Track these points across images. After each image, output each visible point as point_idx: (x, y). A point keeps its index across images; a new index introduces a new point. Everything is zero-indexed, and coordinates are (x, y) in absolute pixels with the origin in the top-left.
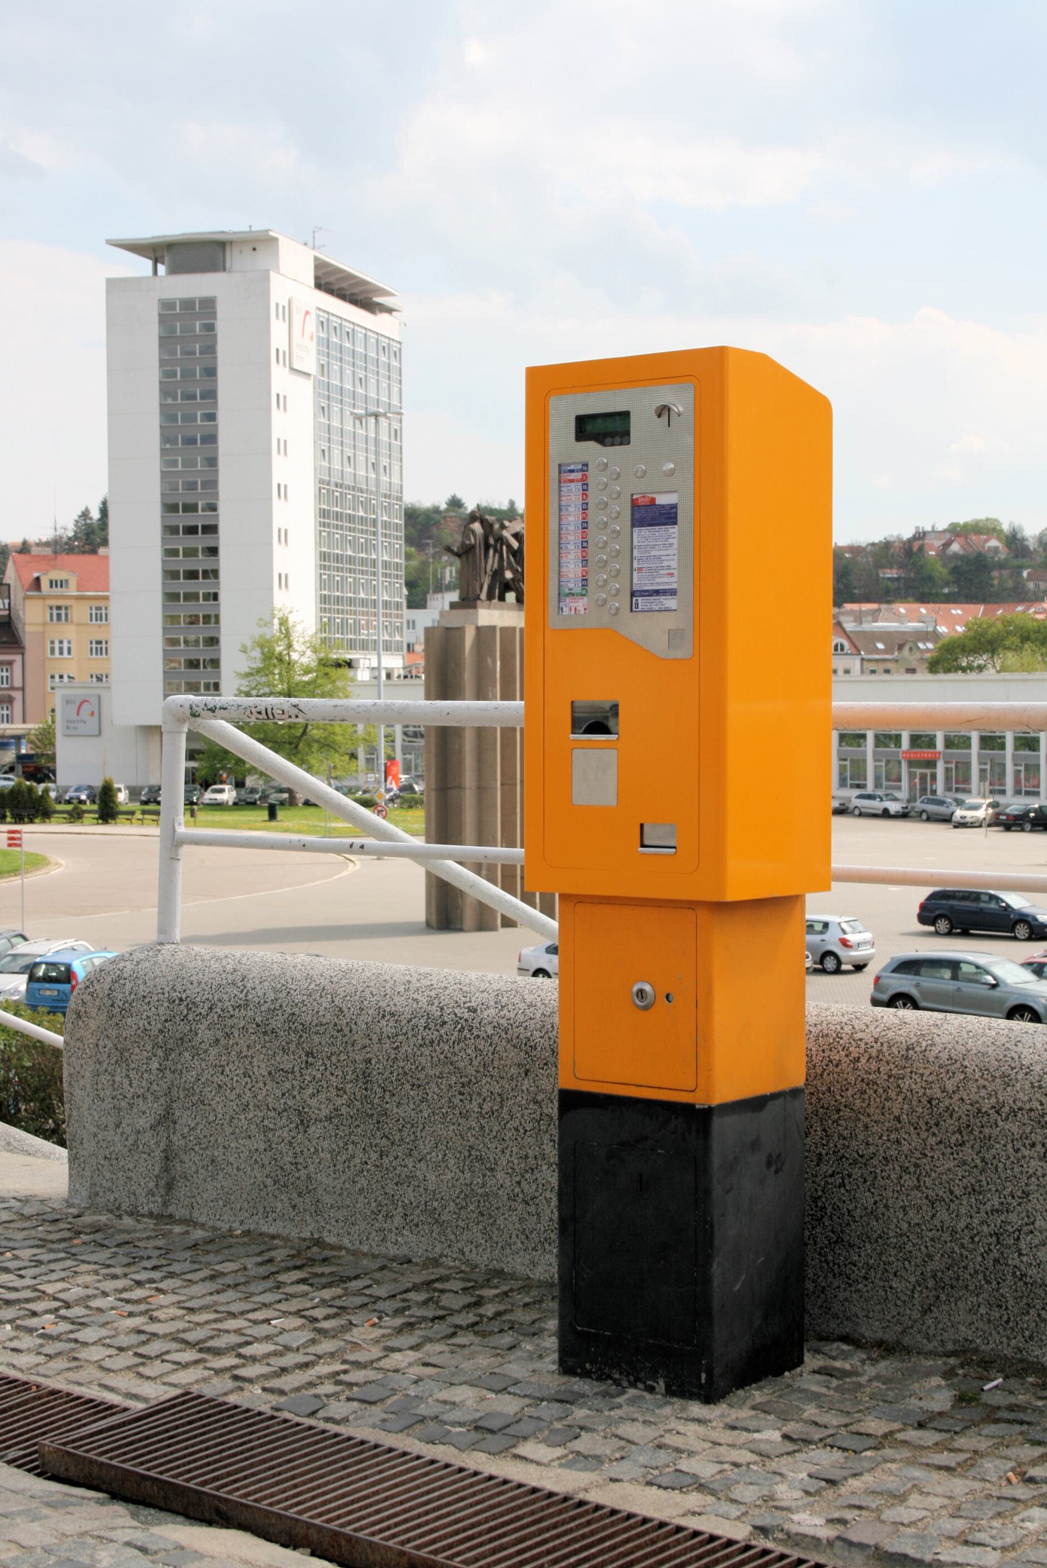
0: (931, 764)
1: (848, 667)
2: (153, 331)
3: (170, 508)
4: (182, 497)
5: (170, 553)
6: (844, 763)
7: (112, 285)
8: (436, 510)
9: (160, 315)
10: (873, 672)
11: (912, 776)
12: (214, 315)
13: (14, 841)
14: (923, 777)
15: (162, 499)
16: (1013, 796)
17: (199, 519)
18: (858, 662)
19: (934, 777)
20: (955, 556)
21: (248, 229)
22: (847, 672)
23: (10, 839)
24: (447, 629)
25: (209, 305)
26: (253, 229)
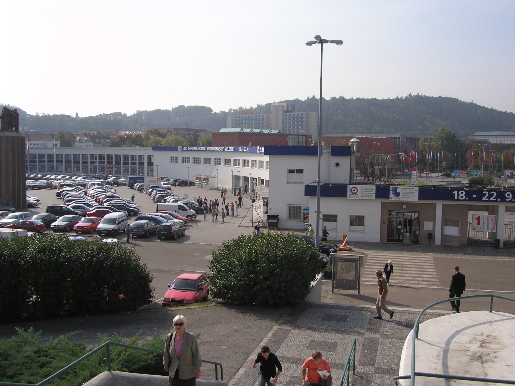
0: (112, 168)
22: (90, 146)
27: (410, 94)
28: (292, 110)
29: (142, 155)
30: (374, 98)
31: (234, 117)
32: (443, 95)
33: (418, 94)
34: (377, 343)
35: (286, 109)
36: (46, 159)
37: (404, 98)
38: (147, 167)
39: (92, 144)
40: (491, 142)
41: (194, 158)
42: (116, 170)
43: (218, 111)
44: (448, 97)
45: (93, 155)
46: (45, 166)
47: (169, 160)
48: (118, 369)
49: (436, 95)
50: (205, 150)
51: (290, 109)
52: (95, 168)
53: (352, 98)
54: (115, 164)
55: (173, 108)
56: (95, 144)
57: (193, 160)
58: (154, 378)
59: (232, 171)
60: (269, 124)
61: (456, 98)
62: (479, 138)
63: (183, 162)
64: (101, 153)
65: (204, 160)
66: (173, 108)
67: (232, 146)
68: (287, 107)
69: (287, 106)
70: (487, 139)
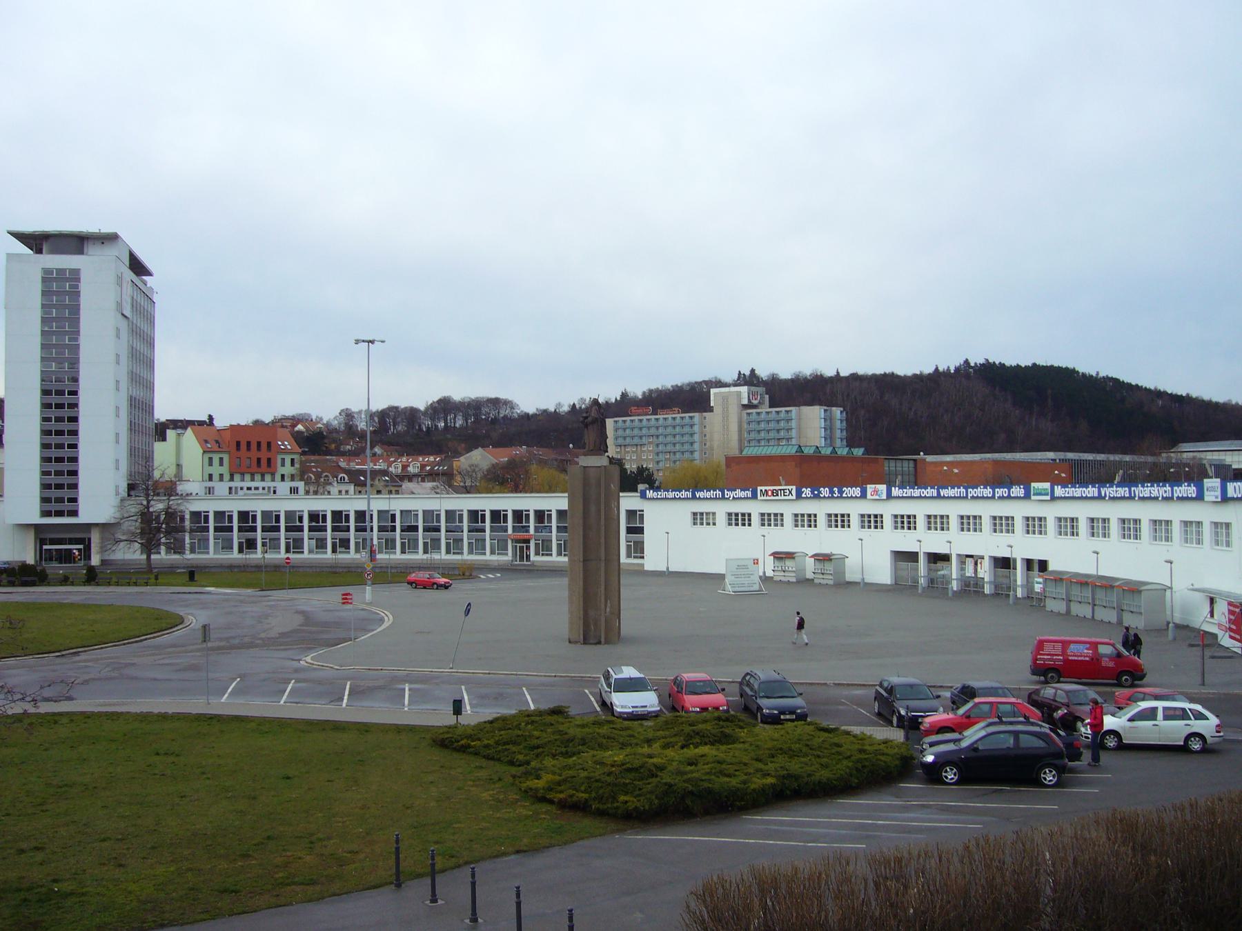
0: (527, 541)
1: (347, 489)
2: (38, 287)
3: (45, 392)
4: (54, 386)
5: (45, 419)
6: (630, 543)
7: (10, 257)
8: (1182, 396)
9: (42, 277)
10: (360, 492)
11: (515, 548)
12: (78, 280)
13: (346, 598)
14: (522, 548)
15: (41, 387)
16: (468, 555)
17: (67, 398)
18: (352, 487)
19: (528, 548)
20: (300, 432)
21: (98, 231)
22: (347, 492)
23: (343, 599)
24: (584, 467)
25: (75, 276)
26: (102, 231)
27: (967, 362)
28: (759, 403)
29: (638, 509)
30: (890, 371)
31: (678, 418)
32: (1042, 362)
33: (987, 360)
34: (1092, 759)
35: (745, 402)
36: (259, 524)
37: (952, 371)
38: (626, 537)
39: (351, 488)
40: (1231, 465)
41: (962, 517)
42: (537, 545)
43: (531, 410)
44: (1052, 366)
45: (477, 512)
46: (439, 540)
47: (689, 518)
48: (654, 776)
49: (1025, 362)
50: (1096, 495)
51: (755, 402)
52: (459, 541)
53: (838, 372)
54: (513, 531)
55: (427, 403)
56: (359, 488)
57: (926, 523)
58: (909, 825)
59: (920, 541)
60: (705, 435)
61: (1070, 366)
62: (1214, 458)
63: (962, 530)
64: (339, 506)
65: (1025, 522)
66: (427, 403)
67: (1149, 482)
68: (749, 397)
69: (749, 394)
70: (1223, 458)
